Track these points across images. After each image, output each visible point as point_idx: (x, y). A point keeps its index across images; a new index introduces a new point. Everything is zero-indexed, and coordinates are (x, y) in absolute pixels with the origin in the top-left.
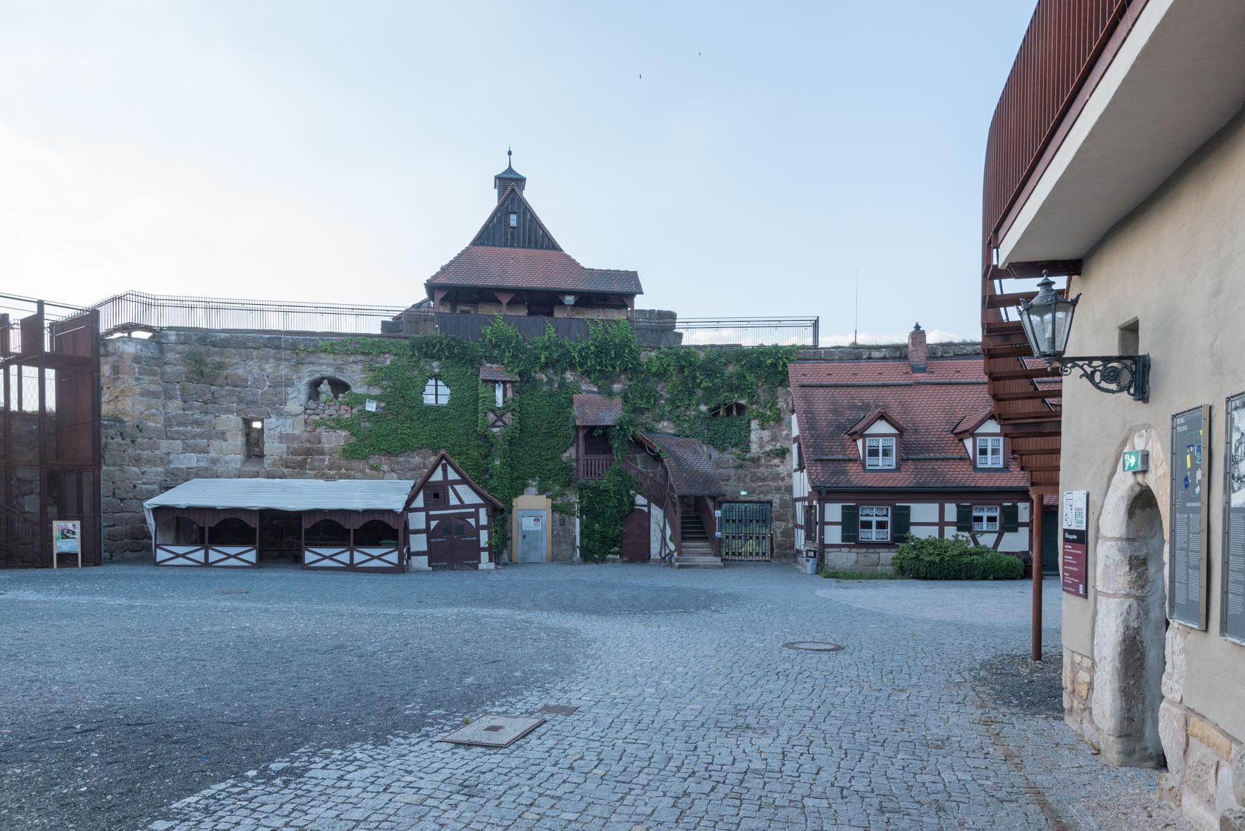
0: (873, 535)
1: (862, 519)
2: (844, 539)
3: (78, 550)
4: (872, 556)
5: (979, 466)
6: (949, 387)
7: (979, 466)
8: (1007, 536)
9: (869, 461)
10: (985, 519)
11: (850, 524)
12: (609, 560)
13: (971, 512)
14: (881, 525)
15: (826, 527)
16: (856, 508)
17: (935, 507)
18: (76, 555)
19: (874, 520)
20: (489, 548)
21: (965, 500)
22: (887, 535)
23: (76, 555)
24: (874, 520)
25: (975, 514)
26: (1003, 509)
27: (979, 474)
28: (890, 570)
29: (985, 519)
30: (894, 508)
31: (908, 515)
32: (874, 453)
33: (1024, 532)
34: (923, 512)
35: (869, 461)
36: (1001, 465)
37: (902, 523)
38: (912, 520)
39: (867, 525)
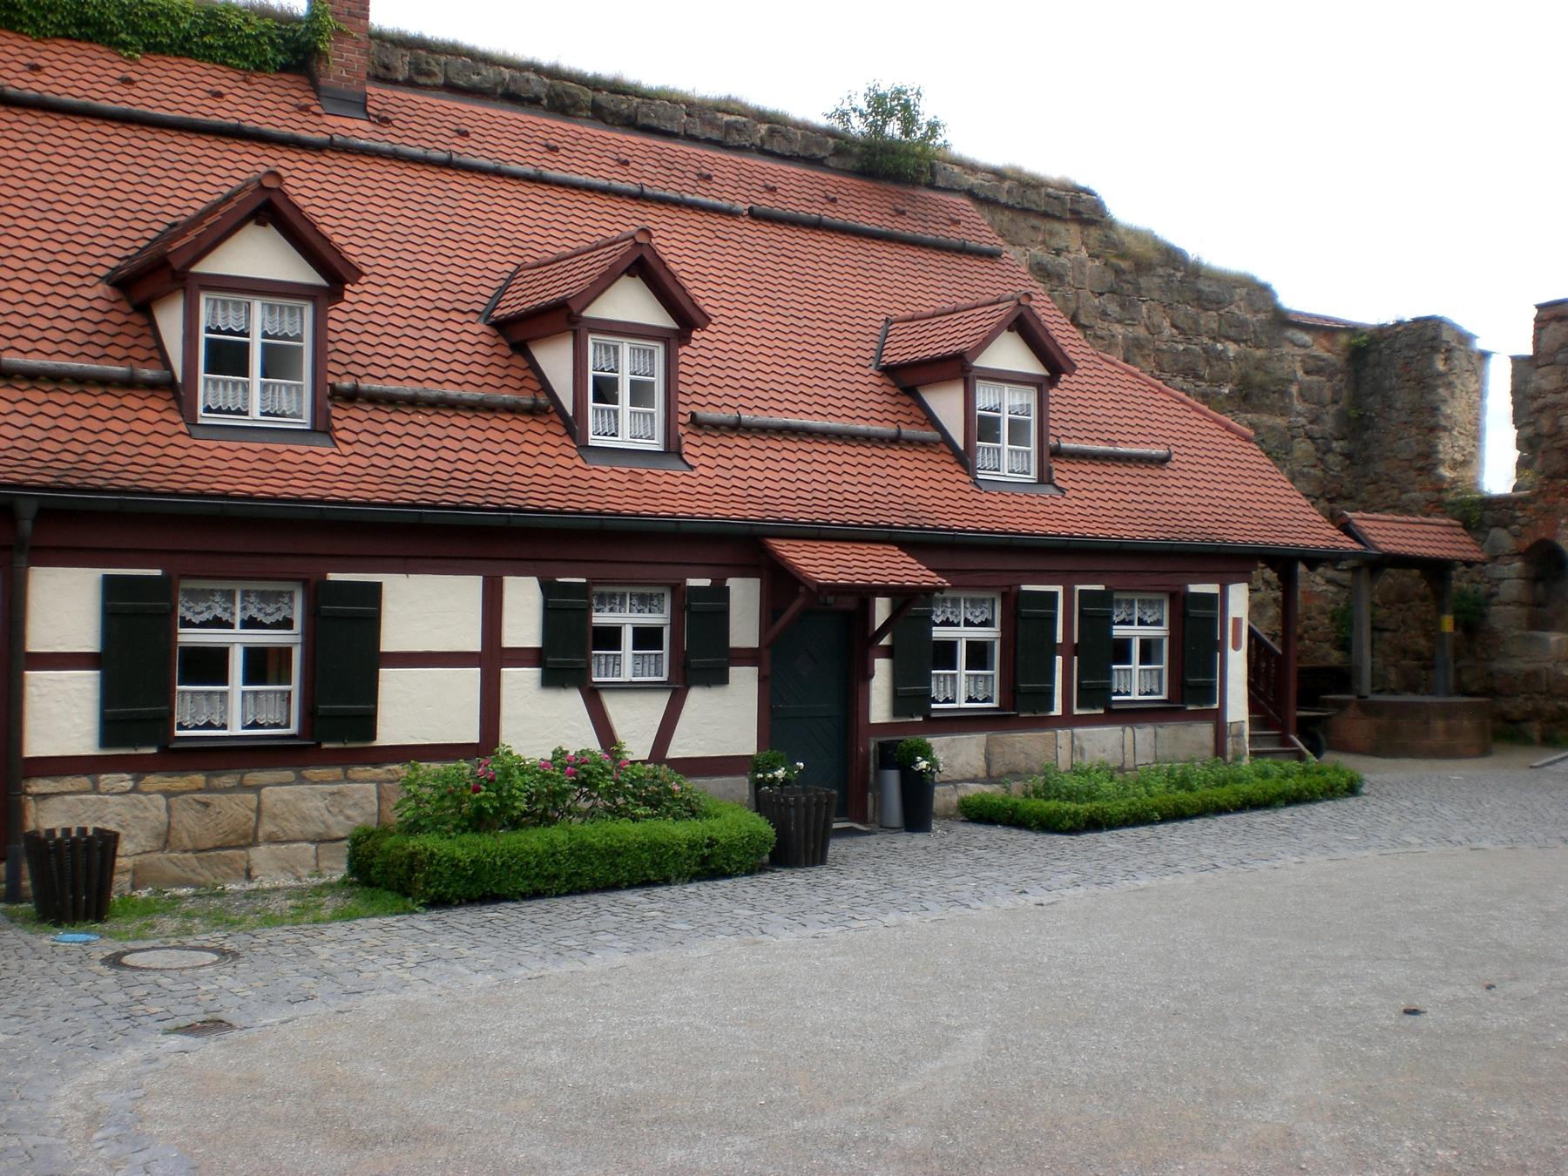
0: (236, 709)
1: (189, 637)
2: (106, 738)
3: (99, 573)
4: (231, 804)
5: (594, 440)
6: (448, 177)
7: (594, 440)
8: (698, 700)
9: (209, 390)
10: (627, 638)
11: (140, 669)
12: (1325, 701)
13: (586, 613)
14: (262, 665)
15: (474, 644)
16: (163, 590)
17: (470, 587)
18: (107, 580)
19: (237, 641)
20: (1070, 650)
21: (573, 563)
22: (276, 710)
23: (106, 578)
24: (237, 641)
25: (601, 618)
26: (684, 601)
27: (603, 472)
28: (733, 814)
29: (627, 638)
30: (320, 597)
31: (372, 622)
32: (228, 357)
33: (745, 681)
34: (425, 609)
35: (209, 390)
36: (656, 444)
37: (345, 661)
38: (388, 644)
39: (210, 665)
